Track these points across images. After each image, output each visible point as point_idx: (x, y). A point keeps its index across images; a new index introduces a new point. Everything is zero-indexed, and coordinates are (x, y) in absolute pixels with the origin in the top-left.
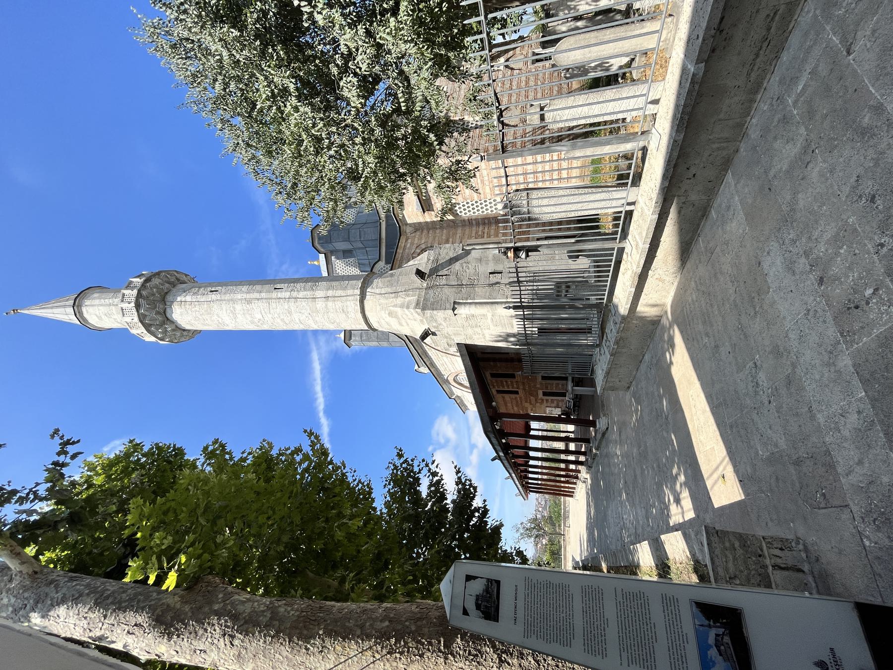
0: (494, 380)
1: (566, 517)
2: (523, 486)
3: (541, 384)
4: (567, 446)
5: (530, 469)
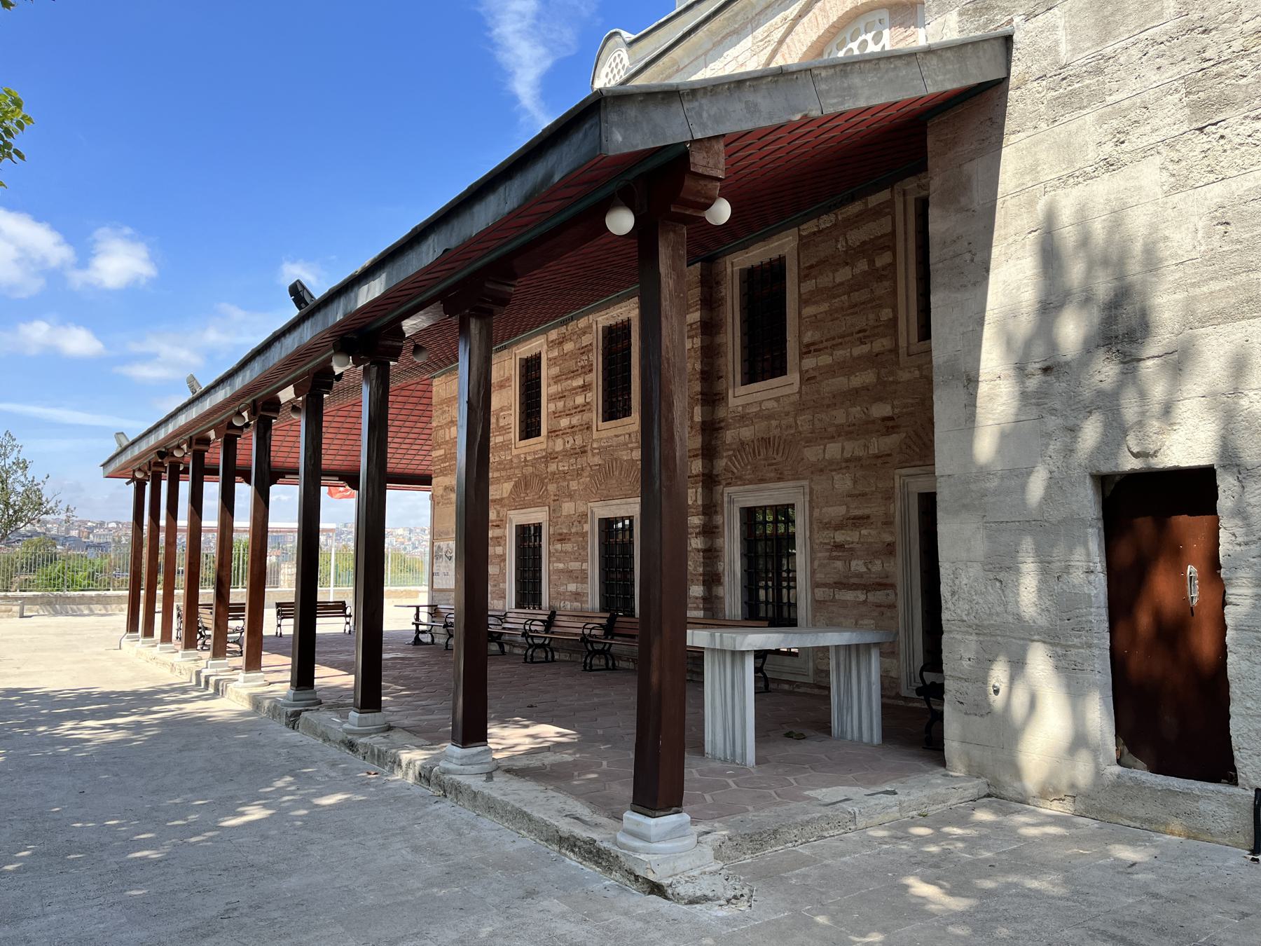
0: (594, 339)
1: (54, 606)
2: (163, 452)
3: (583, 517)
5: (164, 485)
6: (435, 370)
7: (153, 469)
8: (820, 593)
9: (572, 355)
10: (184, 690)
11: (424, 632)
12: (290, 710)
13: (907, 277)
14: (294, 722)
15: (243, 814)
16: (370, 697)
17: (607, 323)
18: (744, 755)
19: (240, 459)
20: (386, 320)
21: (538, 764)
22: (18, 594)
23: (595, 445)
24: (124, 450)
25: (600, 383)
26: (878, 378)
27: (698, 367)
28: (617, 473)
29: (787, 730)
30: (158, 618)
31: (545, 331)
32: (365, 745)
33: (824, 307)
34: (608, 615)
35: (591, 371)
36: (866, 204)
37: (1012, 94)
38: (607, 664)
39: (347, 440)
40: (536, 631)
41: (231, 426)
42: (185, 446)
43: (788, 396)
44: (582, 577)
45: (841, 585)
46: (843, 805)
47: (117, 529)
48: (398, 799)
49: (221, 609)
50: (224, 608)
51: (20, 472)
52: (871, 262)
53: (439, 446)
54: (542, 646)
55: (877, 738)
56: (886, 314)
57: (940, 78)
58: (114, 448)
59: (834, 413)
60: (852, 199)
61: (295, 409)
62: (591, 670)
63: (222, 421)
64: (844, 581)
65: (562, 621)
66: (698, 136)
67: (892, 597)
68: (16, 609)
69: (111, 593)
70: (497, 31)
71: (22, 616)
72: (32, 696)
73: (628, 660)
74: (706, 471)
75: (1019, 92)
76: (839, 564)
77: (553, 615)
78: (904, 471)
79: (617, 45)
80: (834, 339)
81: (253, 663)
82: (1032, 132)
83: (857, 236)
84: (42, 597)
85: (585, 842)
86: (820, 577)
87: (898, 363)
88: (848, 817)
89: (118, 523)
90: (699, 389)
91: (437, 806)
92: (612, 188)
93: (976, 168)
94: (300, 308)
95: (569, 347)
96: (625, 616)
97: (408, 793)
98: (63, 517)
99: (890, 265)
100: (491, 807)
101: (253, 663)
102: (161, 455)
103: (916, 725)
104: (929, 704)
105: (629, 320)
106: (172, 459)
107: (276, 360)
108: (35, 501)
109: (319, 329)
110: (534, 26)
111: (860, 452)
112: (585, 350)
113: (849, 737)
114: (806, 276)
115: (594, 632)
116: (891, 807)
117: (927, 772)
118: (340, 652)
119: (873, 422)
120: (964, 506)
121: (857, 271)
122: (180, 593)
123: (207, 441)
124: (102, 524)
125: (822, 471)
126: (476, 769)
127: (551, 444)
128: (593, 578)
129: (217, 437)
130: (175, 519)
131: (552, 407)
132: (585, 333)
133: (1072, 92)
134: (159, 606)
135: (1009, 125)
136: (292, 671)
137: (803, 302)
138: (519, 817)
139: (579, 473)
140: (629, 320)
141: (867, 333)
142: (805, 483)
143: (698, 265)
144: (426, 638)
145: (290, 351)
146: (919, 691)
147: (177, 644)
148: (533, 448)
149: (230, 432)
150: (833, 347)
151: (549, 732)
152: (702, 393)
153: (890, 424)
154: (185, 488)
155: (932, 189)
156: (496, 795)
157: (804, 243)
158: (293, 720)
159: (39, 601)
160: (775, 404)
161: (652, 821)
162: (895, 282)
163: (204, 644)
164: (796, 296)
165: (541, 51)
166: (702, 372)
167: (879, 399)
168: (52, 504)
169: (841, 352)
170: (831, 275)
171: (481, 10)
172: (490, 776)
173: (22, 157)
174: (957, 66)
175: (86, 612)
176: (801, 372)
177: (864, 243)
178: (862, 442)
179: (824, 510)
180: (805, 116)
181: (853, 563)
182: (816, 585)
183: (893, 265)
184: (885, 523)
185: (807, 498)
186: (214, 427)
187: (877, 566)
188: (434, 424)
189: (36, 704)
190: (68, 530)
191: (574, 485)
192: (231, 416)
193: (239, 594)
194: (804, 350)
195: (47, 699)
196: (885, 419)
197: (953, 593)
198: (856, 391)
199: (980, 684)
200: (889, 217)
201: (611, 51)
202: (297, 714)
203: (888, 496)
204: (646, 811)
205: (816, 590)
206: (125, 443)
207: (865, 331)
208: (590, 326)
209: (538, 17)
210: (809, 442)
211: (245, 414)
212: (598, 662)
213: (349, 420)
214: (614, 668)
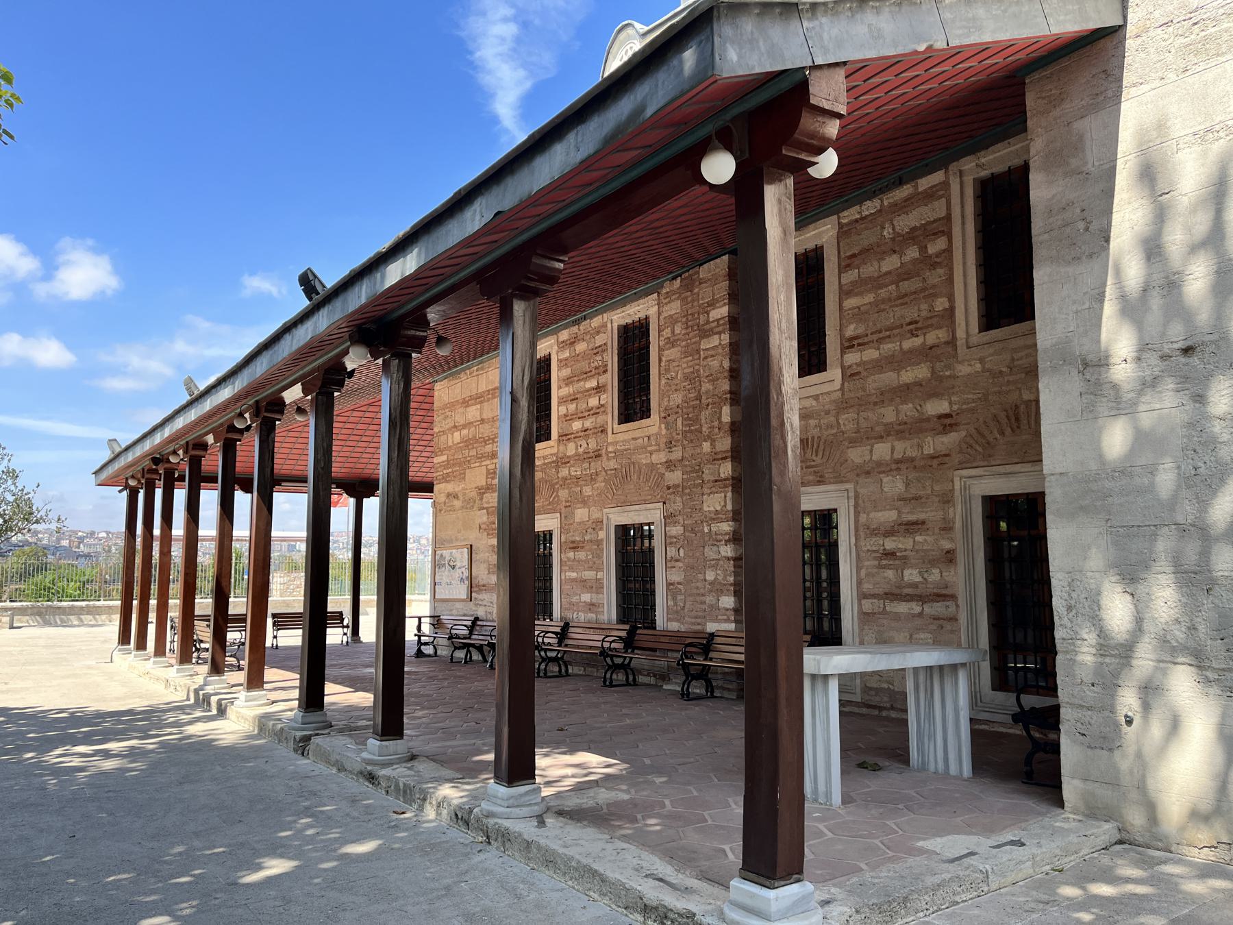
0: (609, 339)
1: (45, 617)
4: (284, 621)
5: (159, 493)
6: (438, 374)
7: (147, 476)
8: (868, 605)
9: (584, 355)
10: (181, 708)
11: (426, 644)
12: (299, 734)
13: (964, 263)
14: (304, 748)
15: (259, 868)
16: (391, 722)
17: (623, 322)
18: (828, 794)
19: (240, 466)
20: (410, 306)
21: (591, 803)
22: (8, 604)
23: (610, 449)
24: (117, 457)
25: (616, 384)
26: (933, 372)
27: (726, 364)
28: (635, 477)
29: (862, 758)
30: (152, 629)
31: (555, 332)
32: (388, 778)
33: (869, 298)
34: (627, 627)
35: (605, 371)
36: (916, 187)
37: (1129, 43)
38: (627, 679)
39: (365, 444)
40: (549, 644)
41: (232, 428)
42: (181, 452)
43: (828, 393)
44: (597, 587)
45: (893, 595)
46: (966, 861)
47: (108, 539)
48: (430, 847)
49: (221, 621)
50: (222, 620)
51: (10, 482)
52: (923, 249)
53: (441, 452)
54: (555, 660)
55: (967, 770)
56: (941, 304)
57: (1062, 18)
58: (106, 455)
59: (883, 411)
60: (900, 182)
61: (300, 411)
62: (611, 685)
63: (222, 425)
64: (897, 591)
65: (575, 633)
66: (819, 61)
67: (952, 609)
68: (6, 619)
69: (101, 603)
70: (478, 54)
71: (12, 627)
72: (23, 716)
73: (648, 675)
74: (736, 475)
75: (1139, 41)
76: (890, 574)
77: (566, 627)
78: (965, 472)
79: (629, 37)
80: (880, 332)
81: (255, 681)
82: (1157, 83)
83: (905, 222)
84: (33, 607)
85: (680, 915)
86: (867, 587)
87: (955, 356)
88: (981, 876)
89: (108, 533)
90: (727, 387)
91: (482, 856)
92: (709, 129)
93: (1090, 126)
94: (310, 299)
95: (581, 347)
96: (645, 628)
97: (444, 838)
98: (54, 526)
99: (944, 251)
100: (549, 860)
101: (255, 681)
102: (156, 461)
103: (1024, 754)
104: (1028, 732)
105: (647, 318)
106: (167, 465)
107: (286, 354)
108: (25, 512)
109: (338, 315)
110: (514, 50)
111: (912, 453)
112: (599, 350)
113: (932, 768)
114: (848, 265)
115: (613, 645)
116: (1024, 862)
117: (1044, 814)
118: (342, 666)
119: (928, 420)
120: (1082, 509)
121: (906, 259)
122: (175, 603)
123: (204, 446)
124: (92, 534)
125: (868, 473)
126: (525, 811)
127: (562, 448)
128: (609, 587)
129: (216, 442)
130: (170, 528)
131: (563, 410)
132: (598, 333)
133: (1206, 38)
134: (152, 617)
135: (1128, 78)
136: (300, 688)
137: (844, 293)
138: (588, 875)
139: (593, 478)
140: (647, 318)
141: (919, 325)
142: (850, 486)
143: (726, 258)
144: (428, 650)
145: (302, 343)
146: (1016, 718)
147: (172, 658)
148: (637, 434)
149: (230, 436)
150: (880, 341)
151: (592, 759)
152: (731, 392)
153: (948, 421)
154: (180, 496)
155: (1033, 152)
156: (555, 846)
157: (844, 232)
158: (303, 745)
159: (29, 611)
160: (814, 403)
161: (772, 894)
162: (951, 269)
163: (199, 658)
164: (836, 287)
165: (522, 73)
166: (731, 370)
167: (934, 394)
168: (42, 513)
169: (890, 346)
170: (876, 264)
171: (463, 34)
172: (541, 823)
173: (12, 137)
174: (1076, 7)
175: (76, 623)
176: (843, 368)
177: (914, 229)
178: (915, 441)
179: (872, 515)
180: (930, 48)
181: (907, 572)
182: (863, 596)
183: (949, 251)
184: (944, 529)
185: (852, 502)
186: (213, 431)
187: (935, 575)
188: (436, 430)
189: (23, 725)
190: (59, 540)
191: (587, 491)
192: (233, 418)
193: (238, 604)
194: (847, 344)
195: (37, 719)
196: (940, 417)
197: (1069, 608)
198: (907, 387)
199: (1107, 713)
200: (944, 200)
201: (623, 44)
202: (307, 739)
203: (947, 499)
204: (762, 880)
205: (864, 602)
206: (118, 450)
207: (916, 322)
208: (604, 326)
209: (518, 40)
210: (854, 442)
211: (247, 415)
212: (619, 677)
213: (348, 426)
214: (635, 683)
